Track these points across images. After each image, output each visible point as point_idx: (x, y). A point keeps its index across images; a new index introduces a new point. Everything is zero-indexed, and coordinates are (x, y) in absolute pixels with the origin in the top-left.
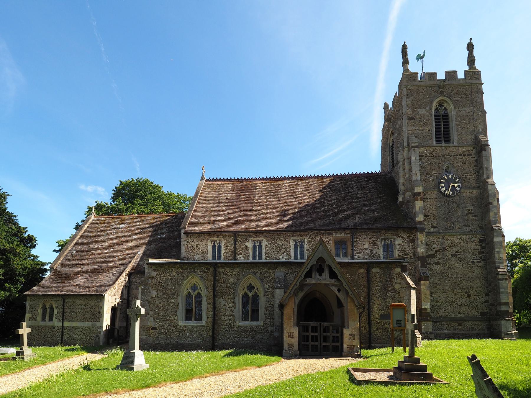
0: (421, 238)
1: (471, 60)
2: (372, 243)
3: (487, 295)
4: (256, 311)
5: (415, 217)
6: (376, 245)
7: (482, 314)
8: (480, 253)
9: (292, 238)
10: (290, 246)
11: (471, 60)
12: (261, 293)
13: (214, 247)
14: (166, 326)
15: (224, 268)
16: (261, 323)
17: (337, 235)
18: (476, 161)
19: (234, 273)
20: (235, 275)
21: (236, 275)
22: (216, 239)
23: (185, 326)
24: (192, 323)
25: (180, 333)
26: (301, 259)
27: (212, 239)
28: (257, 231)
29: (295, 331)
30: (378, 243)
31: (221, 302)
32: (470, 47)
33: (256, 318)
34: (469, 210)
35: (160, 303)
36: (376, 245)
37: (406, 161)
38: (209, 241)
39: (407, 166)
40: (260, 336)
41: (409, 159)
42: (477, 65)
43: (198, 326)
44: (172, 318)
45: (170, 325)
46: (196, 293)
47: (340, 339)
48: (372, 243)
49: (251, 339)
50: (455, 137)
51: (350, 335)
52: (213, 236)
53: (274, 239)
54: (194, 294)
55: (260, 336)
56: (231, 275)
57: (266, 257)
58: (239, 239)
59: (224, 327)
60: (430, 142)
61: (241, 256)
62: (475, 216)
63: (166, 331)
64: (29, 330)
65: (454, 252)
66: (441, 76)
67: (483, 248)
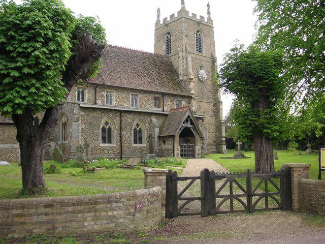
0: (194, 102)
1: (209, 13)
4: (140, 139)
5: (191, 91)
7: (214, 142)
8: (214, 112)
11: (209, 13)
12: (143, 129)
13: (79, 92)
23: (104, 147)
24: (138, 145)
26: (135, 106)
28: (110, 86)
29: (179, 147)
31: (124, 133)
32: (208, 5)
33: (141, 143)
39: (184, 61)
40: (144, 152)
41: (187, 58)
46: (107, 127)
47: (194, 151)
50: (204, 50)
54: (138, 129)
56: (128, 118)
58: (98, 89)
64: (241, 143)
66: (198, 17)
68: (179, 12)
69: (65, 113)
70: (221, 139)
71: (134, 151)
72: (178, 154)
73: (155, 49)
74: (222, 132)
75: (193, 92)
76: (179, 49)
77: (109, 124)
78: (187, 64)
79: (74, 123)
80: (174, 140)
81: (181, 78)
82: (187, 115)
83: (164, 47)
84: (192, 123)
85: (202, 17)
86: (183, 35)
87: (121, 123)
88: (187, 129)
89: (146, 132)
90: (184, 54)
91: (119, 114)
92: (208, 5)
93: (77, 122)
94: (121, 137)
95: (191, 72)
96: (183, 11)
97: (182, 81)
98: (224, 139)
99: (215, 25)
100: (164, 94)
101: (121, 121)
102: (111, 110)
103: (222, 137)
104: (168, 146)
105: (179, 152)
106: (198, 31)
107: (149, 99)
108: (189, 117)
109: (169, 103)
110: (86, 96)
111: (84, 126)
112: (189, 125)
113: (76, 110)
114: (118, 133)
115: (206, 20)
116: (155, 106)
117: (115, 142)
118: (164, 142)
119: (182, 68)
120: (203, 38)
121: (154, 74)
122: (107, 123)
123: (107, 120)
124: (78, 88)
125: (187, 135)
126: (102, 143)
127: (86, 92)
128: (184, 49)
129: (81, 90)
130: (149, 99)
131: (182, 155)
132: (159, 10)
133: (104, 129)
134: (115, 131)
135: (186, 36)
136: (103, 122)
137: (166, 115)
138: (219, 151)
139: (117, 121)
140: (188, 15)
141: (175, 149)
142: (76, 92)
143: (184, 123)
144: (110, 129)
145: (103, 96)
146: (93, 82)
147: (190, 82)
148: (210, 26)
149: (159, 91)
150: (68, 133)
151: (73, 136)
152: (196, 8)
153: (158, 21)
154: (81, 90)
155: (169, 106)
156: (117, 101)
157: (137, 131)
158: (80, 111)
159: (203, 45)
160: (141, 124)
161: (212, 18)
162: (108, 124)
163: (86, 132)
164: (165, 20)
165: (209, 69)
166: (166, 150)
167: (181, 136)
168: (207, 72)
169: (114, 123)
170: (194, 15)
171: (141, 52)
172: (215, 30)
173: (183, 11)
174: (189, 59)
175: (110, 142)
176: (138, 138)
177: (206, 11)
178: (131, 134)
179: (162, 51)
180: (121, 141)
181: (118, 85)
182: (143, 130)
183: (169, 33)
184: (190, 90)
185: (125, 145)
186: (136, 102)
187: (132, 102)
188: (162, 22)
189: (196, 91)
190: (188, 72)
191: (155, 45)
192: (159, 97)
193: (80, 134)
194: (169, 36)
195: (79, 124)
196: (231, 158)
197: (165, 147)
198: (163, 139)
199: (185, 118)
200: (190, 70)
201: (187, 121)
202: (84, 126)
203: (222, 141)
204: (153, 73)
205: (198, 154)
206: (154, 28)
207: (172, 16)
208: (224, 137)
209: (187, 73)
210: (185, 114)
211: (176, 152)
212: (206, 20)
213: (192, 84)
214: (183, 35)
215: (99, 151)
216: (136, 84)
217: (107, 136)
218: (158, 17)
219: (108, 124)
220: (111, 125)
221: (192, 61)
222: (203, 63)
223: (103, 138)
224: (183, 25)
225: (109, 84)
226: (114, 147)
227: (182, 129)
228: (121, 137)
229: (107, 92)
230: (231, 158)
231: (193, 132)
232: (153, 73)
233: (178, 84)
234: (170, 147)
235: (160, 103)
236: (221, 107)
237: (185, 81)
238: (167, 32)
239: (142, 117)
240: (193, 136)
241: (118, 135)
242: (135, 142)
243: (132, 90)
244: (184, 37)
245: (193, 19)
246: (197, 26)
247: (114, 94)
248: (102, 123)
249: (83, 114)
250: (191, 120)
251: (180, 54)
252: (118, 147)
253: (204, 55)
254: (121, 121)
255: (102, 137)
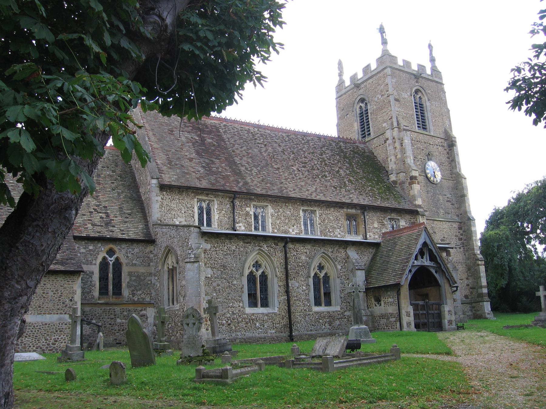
1: (433, 60)
2: (380, 222)
3: (467, 279)
4: (328, 295)
5: (415, 200)
6: (384, 225)
8: (460, 239)
9: (302, 208)
10: (300, 217)
11: (433, 60)
12: (333, 274)
13: (201, 209)
14: (228, 315)
15: (293, 244)
16: (335, 308)
17: (348, 210)
18: (448, 153)
19: (305, 251)
20: (306, 253)
21: (308, 253)
22: (204, 198)
23: (253, 314)
24: (260, 310)
25: (247, 323)
26: (312, 233)
27: (200, 197)
28: (262, 195)
29: (411, 309)
30: (386, 223)
32: (430, 47)
33: (328, 303)
34: (448, 198)
35: (218, 285)
36: (384, 225)
37: (397, 141)
38: (196, 200)
39: (397, 145)
40: (337, 322)
42: (437, 64)
43: (270, 313)
44: (236, 304)
45: (233, 314)
46: (260, 272)
47: (440, 316)
48: (380, 222)
49: (329, 327)
51: (449, 311)
52: (201, 194)
53: (281, 208)
54: (322, 275)
55: (337, 322)
56: (301, 254)
57: (273, 228)
58: (237, 203)
59: (299, 314)
60: (414, 126)
61: (241, 224)
62: (453, 204)
63: (229, 321)
65: (442, 237)
67: (462, 235)
68: (380, 61)
69: (173, 248)
70: (480, 290)
71: (317, 321)
72: (409, 324)
73: (339, 131)
74: (480, 277)
75: (419, 202)
76: (384, 125)
77: (263, 266)
78: (403, 151)
79: (189, 266)
80: (399, 294)
81: (393, 178)
82: (421, 241)
83: (356, 126)
84: (433, 258)
85: (421, 67)
86: (391, 98)
87: (286, 264)
88: (422, 270)
89: (338, 281)
90: (396, 132)
91: (281, 245)
92: (430, 47)
93: (196, 265)
94: (287, 292)
95: (412, 165)
96: (386, 59)
97: (395, 182)
98: (485, 291)
99: (445, 80)
100: (364, 208)
101: (286, 258)
102: (265, 238)
103: (481, 287)
104: (387, 307)
105: (412, 318)
106: (417, 92)
107: (337, 219)
108: (425, 244)
109: (376, 225)
110: (215, 216)
111: (209, 272)
112: (426, 262)
113: (194, 240)
114: (282, 270)
115: (429, 72)
116: (350, 232)
117: (277, 304)
118: (378, 300)
119: (393, 158)
120: (427, 104)
121: (342, 172)
122: (257, 265)
123: (259, 258)
124: (199, 201)
125: (425, 282)
126: (249, 306)
127: (215, 207)
128: (395, 124)
129: (204, 205)
130: (337, 219)
131: (417, 326)
132: (340, 64)
133: (251, 278)
134: (276, 280)
135: (397, 100)
136: (250, 262)
137: (376, 245)
138: (478, 316)
139: (278, 258)
140: (396, 63)
141: (403, 312)
142: (196, 210)
143: (416, 259)
144: (264, 277)
145: (247, 214)
146: (228, 189)
147: (411, 184)
148: (437, 82)
149: (355, 201)
150: (179, 288)
151: (188, 294)
152: (411, 54)
153: (341, 83)
154: (204, 205)
155: (375, 230)
156: (273, 221)
157: (319, 280)
158: (202, 241)
159: (429, 115)
160: (326, 265)
161: (440, 68)
162: (260, 266)
163: (215, 284)
164: (353, 78)
165: (444, 158)
166: (382, 316)
167: (414, 284)
168: (440, 165)
169: (272, 266)
170: (407, 63)
171: (315, 135)
172: (446, 88)
173: (386, 59)
174: (407, 141)
175: (265, 304)
176: (322, 292)
177: (428, 58)
178: (308, 285)
179: (354, 132)
180: (289, 301)
181: (275, 191)
182: (331, 278)
183: (362, 100)
184: (414, 198)
185: (298, 308)
186: (312, 225)
187: (305, 225)
188: (348, 83)
189: (423, 201)
190: (406, 165)
191: (338, 125)
192: (357, 212)
193: (203, 289)
194: (363, 105)
195: (199, 266)
196: (527, 327)
197: (378, 310)
198: (375, 292)
199: (419, 246)
200: (410, 161)
201: (421, 253)
202: (209, 272)
203: (481, 295)
204: (341, 171)
205: (450, 322)
206: (334, 95)
207: (367, 69)
208: (484, 287)
209: (404, 167)
210: (417, 240)
211: (405, 320)
212: (429, 72)
213: (416, 187)
214: (391, 98)
215: (243, 325)
216: (311, 191)
217: (258, 291)
218: (340, 75)
219: (260, 266)
220: (266, 267)
221: (413, 145)
222: (433, 149)
223: (252, 296)
224: (389, 80)
225: (259, 191)
226: (275, 314)
227: (413, 271)
228: (287, 292)
229: (256, 207)
230: (527, 327)
231: (437, 276)
232: (341, 171)
233: (390, 189)
234: (392, 309)
235: (357, 226)
236: (473, 229)
237: (403, 183)
238: (359, 100)
239: (329, 250)
240: (437, 284)
241: (282, 290)
242: (318, 303)
243: (304, 201)
244: (393, 102)
245: (406, 70)
246: (413, 82)
247: (270, 210)
248: (247, 266)
249: (208, 246)
250: (430, 251)
251: (388, 134)
252: (284, 313)
253: (432, 134)
254: (286, 258)
255: (250, 295)
